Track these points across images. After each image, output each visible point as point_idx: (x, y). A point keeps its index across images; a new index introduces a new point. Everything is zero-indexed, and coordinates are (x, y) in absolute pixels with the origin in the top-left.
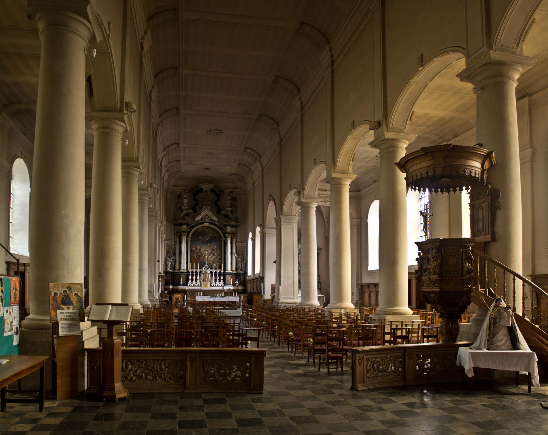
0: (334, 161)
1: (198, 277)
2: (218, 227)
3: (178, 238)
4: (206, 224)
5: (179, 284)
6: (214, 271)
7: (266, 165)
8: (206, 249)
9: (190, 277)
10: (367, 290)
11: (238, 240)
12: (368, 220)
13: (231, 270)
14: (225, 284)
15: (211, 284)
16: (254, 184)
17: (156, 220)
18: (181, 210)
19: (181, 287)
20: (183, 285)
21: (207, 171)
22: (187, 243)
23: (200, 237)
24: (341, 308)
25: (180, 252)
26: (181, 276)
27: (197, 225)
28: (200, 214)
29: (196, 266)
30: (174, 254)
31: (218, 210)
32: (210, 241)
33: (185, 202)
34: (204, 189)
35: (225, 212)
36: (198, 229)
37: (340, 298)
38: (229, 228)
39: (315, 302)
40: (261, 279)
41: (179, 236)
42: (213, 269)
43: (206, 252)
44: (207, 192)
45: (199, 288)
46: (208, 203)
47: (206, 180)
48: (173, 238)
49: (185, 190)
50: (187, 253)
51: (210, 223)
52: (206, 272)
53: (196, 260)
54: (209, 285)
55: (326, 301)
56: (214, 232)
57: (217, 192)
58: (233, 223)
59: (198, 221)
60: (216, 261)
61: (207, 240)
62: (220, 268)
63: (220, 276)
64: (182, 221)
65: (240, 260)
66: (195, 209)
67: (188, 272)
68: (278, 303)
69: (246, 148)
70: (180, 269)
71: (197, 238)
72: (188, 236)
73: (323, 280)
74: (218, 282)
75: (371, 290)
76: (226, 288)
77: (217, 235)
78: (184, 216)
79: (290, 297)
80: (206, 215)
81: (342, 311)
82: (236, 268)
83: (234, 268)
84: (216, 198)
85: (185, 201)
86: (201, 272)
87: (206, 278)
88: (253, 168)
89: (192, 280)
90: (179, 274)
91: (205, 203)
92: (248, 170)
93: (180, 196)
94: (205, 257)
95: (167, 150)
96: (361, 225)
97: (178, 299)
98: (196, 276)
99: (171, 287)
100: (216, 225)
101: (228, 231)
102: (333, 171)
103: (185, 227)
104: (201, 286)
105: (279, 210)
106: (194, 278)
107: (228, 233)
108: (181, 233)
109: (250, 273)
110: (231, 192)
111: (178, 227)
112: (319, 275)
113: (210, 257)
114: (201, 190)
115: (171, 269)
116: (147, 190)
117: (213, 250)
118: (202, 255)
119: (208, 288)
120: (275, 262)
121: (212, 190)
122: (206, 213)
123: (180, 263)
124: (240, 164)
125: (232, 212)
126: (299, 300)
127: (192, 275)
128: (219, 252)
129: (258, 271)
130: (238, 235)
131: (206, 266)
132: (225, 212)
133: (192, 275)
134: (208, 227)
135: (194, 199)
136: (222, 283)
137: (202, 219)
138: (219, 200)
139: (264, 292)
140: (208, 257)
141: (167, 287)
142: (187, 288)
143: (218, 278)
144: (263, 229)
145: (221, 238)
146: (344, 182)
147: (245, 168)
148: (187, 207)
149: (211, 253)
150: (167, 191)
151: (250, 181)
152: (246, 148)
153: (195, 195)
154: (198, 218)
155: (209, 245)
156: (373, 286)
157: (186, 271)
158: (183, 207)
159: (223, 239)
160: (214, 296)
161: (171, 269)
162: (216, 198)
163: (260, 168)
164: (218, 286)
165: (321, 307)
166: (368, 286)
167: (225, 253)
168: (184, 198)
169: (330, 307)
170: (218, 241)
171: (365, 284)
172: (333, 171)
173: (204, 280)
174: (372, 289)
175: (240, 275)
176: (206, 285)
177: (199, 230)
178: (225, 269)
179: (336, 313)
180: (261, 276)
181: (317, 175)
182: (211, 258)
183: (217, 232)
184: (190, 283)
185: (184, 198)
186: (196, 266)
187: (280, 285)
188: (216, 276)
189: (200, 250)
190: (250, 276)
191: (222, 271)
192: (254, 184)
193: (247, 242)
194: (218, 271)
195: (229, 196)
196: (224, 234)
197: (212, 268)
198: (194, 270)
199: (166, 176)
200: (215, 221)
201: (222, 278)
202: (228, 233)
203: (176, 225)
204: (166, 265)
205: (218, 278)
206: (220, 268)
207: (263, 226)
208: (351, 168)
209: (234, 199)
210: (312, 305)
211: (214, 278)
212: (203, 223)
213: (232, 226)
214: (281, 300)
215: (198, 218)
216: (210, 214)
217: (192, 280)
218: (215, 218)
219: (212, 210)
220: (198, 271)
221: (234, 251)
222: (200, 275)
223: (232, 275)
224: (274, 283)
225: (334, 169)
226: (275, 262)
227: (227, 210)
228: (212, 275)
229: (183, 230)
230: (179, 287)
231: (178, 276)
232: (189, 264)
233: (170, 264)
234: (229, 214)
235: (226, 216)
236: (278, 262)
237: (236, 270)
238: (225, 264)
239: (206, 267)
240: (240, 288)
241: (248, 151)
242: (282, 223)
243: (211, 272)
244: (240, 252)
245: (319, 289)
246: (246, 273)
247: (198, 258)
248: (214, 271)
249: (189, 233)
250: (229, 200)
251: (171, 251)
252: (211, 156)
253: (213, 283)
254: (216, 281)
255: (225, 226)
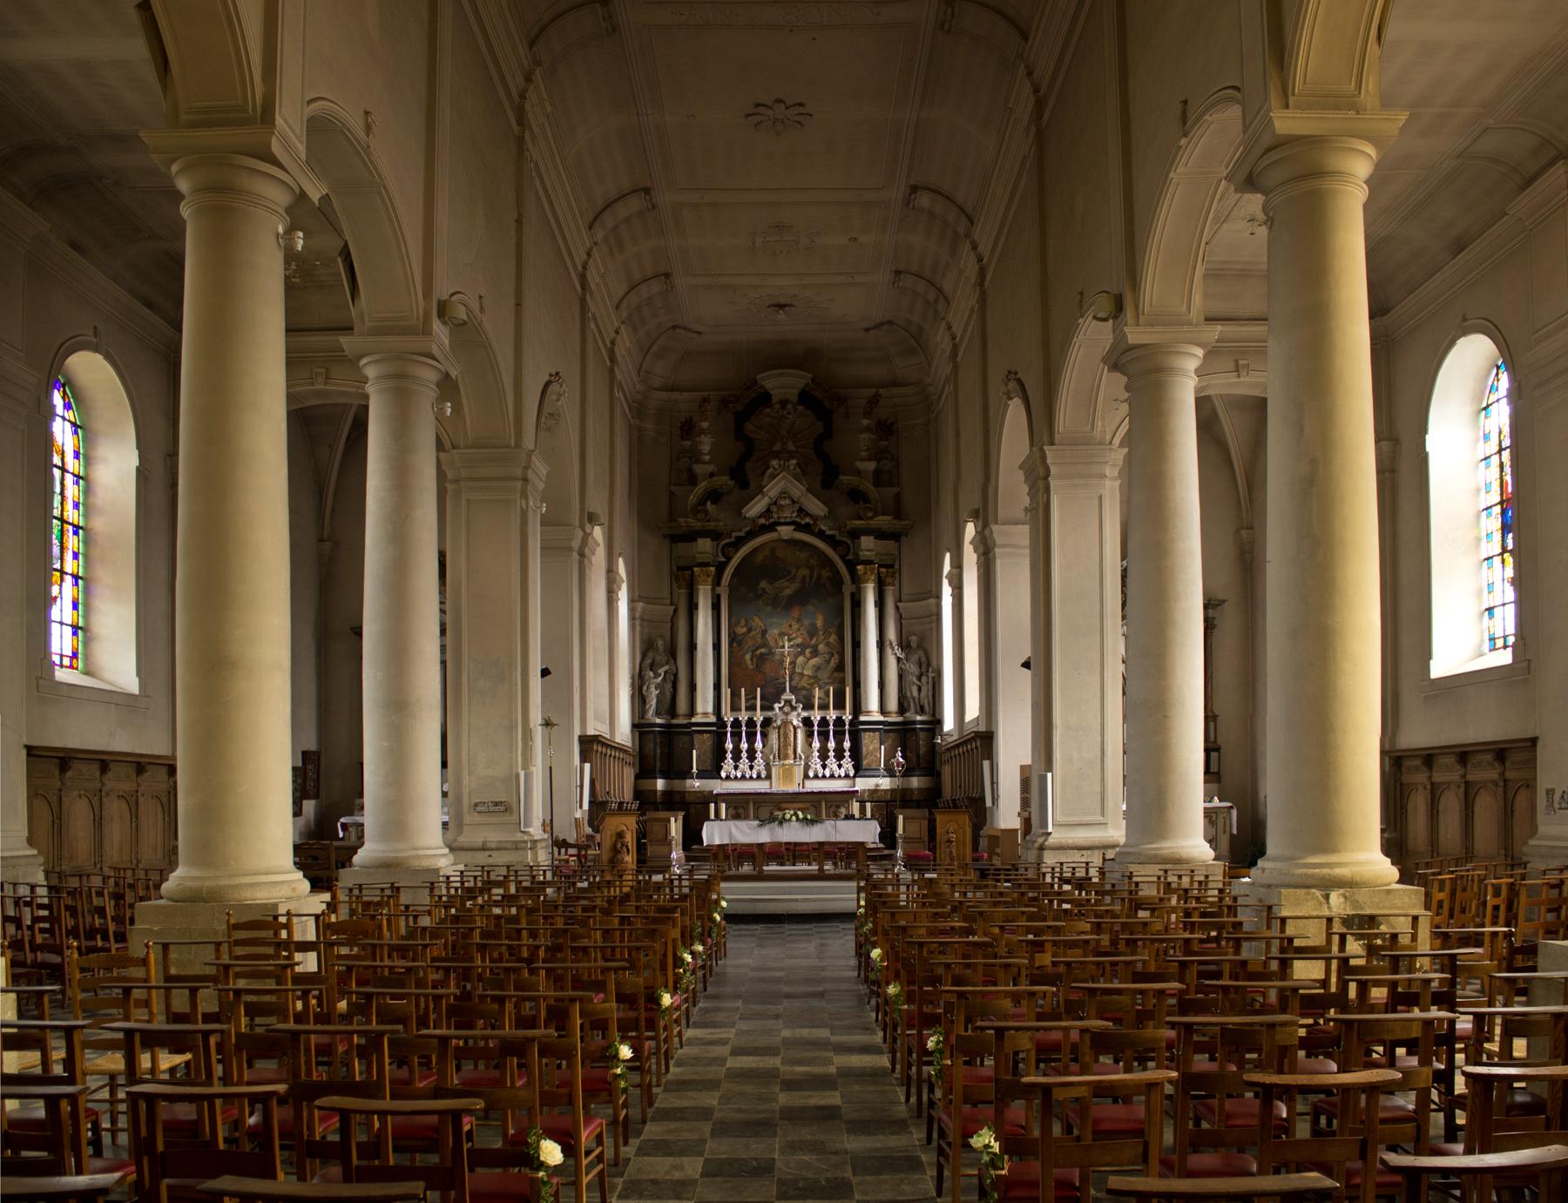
0: (1280, 49)
1: (759, 745)
2: (830, 540)
3: (683, 591)
4: (785, 531)
5: (686, 774)
6: (816, 716)
7: (993, 251)
8: (785, 629)
9: (729, 746)
10: (1420, 777)
11: (905, 591)
12: (1428, 437)
13: (883, 711)
14: (858, 768)
15: (807, 767)
16: (955, 348)
17: (524, 495)
18: (692, 480)
19: (697, 783)
20: (700, 776)
21: (781, 316)
22: (716, 607)
23: (763, 584)
24: (1328, 885)
25: (692, 647)
26: (697, 737)
27: (751, 535)
28: (760, 490)
29: (751, 697)
30: (673, 654)
31: (826, 473)
32: (799, 599)
33: (706, 448)
34: (777, 395)
35: (854, 479)
36: (754, 551)
37: (1322, 829)
38: (867, 542)
39: (1193, 842)
40: (982, 741)
41: (685, 578)
42: (812, 707)
43: (789, 642)
44: (784, 403)
45: (762, 787)
46: (791, 447)
47: (784, 356)
48: (666, 594)
49: (705, 400)
50: (717, 647)
51: (799, 527)
52: (786, 723)
53: (751, 675)
54: (798, 772)
55: (1243, 845)
56: (813, 562)
57: (822, 403)
58: (883, 521)
59: (753, 520)
60: (824, 676)
61: (788, 592)
62: (840, 705)
63: (839, 736)
64: (695, 524)
65: (912, 668)
66: (743, 474)
67: (721, 723)
68: (1042, 848)
69: (914, 189)
70: (692, 712)
71: (752, 586)
72: (717, 582)
73: (1229, 735)
74: (832, 762)
75: (1438, 777)
76: (862, 784)
77: (825, 573)
78: (702, 502)
79: (1084, 820)
80: (784, 494)
81: (1335, 897)
82: (901, 704)
83: (893, 704)
84: (819, 427)
85: (706, 445)
86: (767, 722)
87: (786, 745)
88: (947, 286)
89: (737, 756)
90: (689, 731)
91: (777, 447)
92: (931, 297)
93: (688, 429)
94: (782, 662)
95: (609, 220)
96: (1393, 471)
97: (620, 835)
98: (751, 738)
99: (660, 784)
100: (821, 535)
101: (864, 555)
102: (1274, 100)
103: (705, 545)
104: (769, 777)
105: (1042, 426)
106: (744, 746)
107: (868, 562)
108: (690, 568)
109: (949, 724)
110: (874, 401)
111: (682, 548)
112: (1210, 718)
113: (801, 659)
114: (765, 398)
115: (658, 714)
116: (427, 331)
117: (812, 632)
118: (771, 653)
119: (793, 788)
120: (1026, 665)
121: (805, 397)
122: (782, 488)
123: (692, 687)
124: (898, 273)
125: (878, 478)
126: (1116, 832)
127: (737, 736)
128: (833, 638)
129: (973, 710)
130: (905, 570)
131: (788, 695)
132: (854, 479)
133: (737, 736)
134: (792, 542)
135: (740, 434)
136: (848, 764)
137: (767, 512)
138: (828, 434)
139: (995, 799)
140: (793, 663)
141: (645, 784)
142: (718, 787)
143: (832, 745)
144: (986, 525)
145: (842, 582)
146: (1336, 161)
147: (921, 287)
148: (711, 468)
149: (803, 646)
150: (638, 408)
151: (940, 341)
152: (914, 189)
153: (741, 418)
154: (755, 509)
155: (796, 612)
156: (1451, 760)
157: (713, 719)
158: (699, 469)
159: (848, 588)
160: (772, 819)
161: (658, 714)
162: (819, 427)
163: (971, 269)
164: (834, 778)
165: (1218, 878)
166: (1429, 758)
167: (857, 645)
168: (702, 432)
169: (1265, 878)
170: (829, 594)
171: (1413, 753)
172: (1274, 100)
173: (782, 755)
174: (118, 782)
175: (914, 735)
176: (788, 774)
177: (760, 557)
178: (857, 709)
179: (1306, 918)
180: (982, 728)
181: (1199, 222)
182: (807, 665)
183: (826, 562)
184: (728, 766)
185: (702, 432)
186: (751, 697)
187: (1049, 766)
188: (824, 736)
189: (764, 632)
190: (948, 734)
191: (848, 717)
192: (955, 348)
193: (939, 597)
194: (832, 715)
195: (867, 414)
196: (851, 567)
197: (808, 706)
198: (743, 717)
199: (624, 344)
200: (815, 518)
201: (847, 745)
202: (868, 562)
203: (675, 539)
204: (639, 698)
205: (832, 745)
206: (840, 705)
207: (984, 516)
208: (1370, 84)
209: (885, 429)
210: (1178, 861)
211: (816, 744)
212: (771, 528)
213: (880, 535)
214: (1057, 836)
215: (755, 509)
216: (798, 490)
217: (737, 756)
218: (816, 507)
219: (803, 473)
220: (759, 717)
221: (891, 634)
222: (764, 735)
223: (886, 729)
224: (1028, 762)
225: (1285, 93)
226: (1026, 665)
227: (859, 473)
228: (810, 735)
229: (701, 558)
230: (689, 782)
231: (686, 739)
232: (726, 692)
233: (654, 693)
234: (868, 486)
235: (856, 495)
236: (1040, 664)
237: (902, 709)
238: (857, 685)
239: (788, 702)
240: (915, 782)
241: (924, 200)
242: (1053, 483)
243: (807, 722)
244: (914, 639)
245: (1210, 774)
246: (937, 722)
247: (758, 668)
248: (816, 716)
249: (721, 568)
250: (868, 429)
251: (660, 643)
252: (792, 252)
253: (816, 763)
254: (824, 756)
255: (855, 534)
